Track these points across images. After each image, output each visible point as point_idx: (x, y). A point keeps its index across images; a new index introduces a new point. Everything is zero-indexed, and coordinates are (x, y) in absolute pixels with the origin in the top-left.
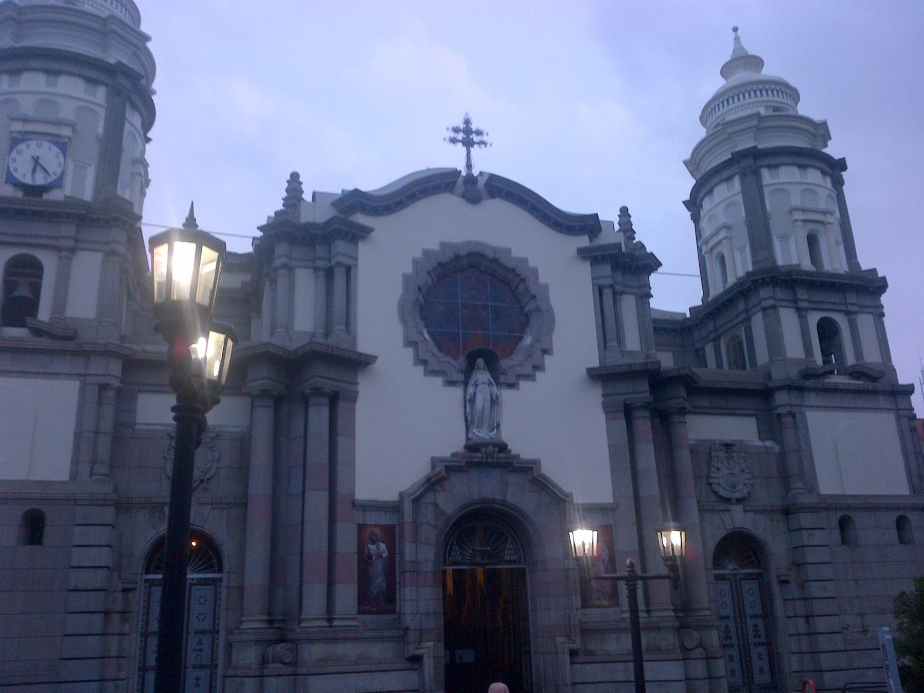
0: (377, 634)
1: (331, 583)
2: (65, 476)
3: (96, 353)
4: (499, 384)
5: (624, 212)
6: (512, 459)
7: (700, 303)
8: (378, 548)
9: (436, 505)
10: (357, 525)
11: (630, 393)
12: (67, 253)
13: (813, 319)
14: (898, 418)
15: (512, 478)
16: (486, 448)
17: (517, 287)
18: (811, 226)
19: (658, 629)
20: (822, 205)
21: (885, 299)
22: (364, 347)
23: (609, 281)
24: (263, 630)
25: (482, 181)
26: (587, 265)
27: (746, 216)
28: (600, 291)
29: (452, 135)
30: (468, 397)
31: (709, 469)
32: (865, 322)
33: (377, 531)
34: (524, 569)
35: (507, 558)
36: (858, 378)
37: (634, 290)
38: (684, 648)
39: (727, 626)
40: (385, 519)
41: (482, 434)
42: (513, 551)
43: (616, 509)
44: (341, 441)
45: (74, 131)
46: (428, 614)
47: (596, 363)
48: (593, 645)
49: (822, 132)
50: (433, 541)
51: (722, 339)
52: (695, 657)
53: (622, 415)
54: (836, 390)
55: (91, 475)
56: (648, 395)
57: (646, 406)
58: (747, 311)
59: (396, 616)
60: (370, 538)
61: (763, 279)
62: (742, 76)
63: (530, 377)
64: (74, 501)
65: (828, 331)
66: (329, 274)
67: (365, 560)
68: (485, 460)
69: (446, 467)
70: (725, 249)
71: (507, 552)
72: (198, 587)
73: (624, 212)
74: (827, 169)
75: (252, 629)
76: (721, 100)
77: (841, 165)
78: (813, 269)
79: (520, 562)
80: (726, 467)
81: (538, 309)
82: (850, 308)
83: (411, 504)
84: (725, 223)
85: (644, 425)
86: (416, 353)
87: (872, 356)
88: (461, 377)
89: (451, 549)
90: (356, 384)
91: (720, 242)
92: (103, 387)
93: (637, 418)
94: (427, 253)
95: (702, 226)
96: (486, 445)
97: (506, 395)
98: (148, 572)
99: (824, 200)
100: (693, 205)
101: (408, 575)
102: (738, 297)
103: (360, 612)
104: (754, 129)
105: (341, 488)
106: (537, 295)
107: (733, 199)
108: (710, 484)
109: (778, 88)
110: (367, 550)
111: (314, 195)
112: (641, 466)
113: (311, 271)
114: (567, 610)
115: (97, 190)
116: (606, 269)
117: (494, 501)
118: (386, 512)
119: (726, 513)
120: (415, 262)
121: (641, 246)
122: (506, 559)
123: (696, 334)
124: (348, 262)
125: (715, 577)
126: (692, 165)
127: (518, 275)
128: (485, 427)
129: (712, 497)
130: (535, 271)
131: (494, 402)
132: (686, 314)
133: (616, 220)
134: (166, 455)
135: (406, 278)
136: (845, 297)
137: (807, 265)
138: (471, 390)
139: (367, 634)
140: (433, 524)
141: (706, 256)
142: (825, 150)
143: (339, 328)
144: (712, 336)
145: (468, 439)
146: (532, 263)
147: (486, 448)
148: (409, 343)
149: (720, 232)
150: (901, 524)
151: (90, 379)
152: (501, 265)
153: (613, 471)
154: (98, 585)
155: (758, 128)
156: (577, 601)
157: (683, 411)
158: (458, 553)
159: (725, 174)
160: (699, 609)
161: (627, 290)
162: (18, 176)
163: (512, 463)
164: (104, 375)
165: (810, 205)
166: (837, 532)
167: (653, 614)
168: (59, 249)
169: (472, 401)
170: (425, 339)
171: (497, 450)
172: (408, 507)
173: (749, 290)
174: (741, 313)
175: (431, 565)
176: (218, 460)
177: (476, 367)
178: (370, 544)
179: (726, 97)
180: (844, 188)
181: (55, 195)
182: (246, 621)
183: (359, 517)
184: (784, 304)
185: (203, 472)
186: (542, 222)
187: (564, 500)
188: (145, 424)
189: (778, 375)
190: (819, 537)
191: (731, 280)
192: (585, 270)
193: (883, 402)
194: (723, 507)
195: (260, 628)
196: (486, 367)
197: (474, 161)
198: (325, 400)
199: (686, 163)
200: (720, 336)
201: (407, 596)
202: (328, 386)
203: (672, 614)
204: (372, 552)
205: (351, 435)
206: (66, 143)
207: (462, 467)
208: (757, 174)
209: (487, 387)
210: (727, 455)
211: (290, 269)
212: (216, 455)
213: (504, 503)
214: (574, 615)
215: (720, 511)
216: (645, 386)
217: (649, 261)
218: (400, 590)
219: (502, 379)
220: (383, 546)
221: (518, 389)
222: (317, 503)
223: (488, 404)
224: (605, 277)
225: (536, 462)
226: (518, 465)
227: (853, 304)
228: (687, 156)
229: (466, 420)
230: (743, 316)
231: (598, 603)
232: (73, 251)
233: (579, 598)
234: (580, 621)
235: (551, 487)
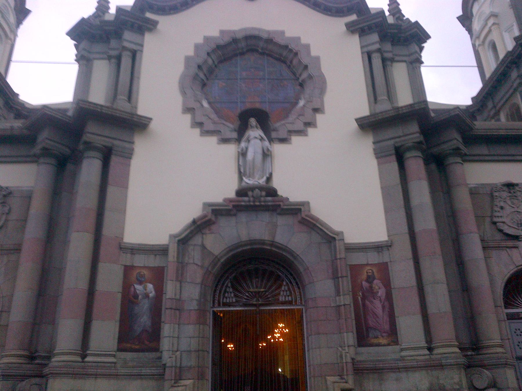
0: (135, 371)
6: (281, 201)
8: (145, 288)
9: (203, 247)
10: (123, 267)
11: (400, 137)
15: (281, 221)
16: (252, 191)
17: (291, 62)
19: (441, 367)
22: (143, 110)
26: (356, 38)
31: (492, 208)
35: (281, 299)
40: (153, 262)
42: (288, 292)
43: (390, 246)
44: (111, 191)
46: (190, 351)
47: (364, 111)
50: (199, 280)
53: (394, 158)
57: (417, 146)
60: (137, 279)
68: (252, 204)
69: (213, 211)
80: (510, 206)
81: (310, 77)
84: (492, 12)
86: (193, 118)
88: (235, 135)
89: (225, 292)
90: (133, 143)
91: (490, 31)
93: (408, 158)
94: (207, 39)
97: (278, 149)
102: (510, 68)
105: (107, 231)
106: (308, 64)
108: (495, 223)
112: (415, 202)
114: (340, 348)
117: (262, 242)
118: (156, 255)
119: (515, 250)
125: (507, 316)
127: (291, 51)
129: (498, 236)
130: (307, 47)
131: (266, 155)
135: (188, 59)
139: (123, 371)
140: (199, 264)
143: (122, 97)
146: (304, 41)
147: (252, 191)
148: (188, 110)
152: (276, 44)
156: (350, 338)
158: (232, 295)
160: (488, 347)
161: (397, 58)
167: (435, 351)
171: (264, 193)
174: (515, 80)
175: (195, 303)
176: (7, 214)
177: (249, 126)
178: (137, 284)
183: (127, 259)
186: (314, 9)
187: (334, 238)
191: (501, 56)
192: (355, 40)
194: (510, 243)
195: (15, 363)
196: (259, 126)
200: (499, 111)
202: (99, 141)
203: (457, 350)
204: (138, 292)
205: (124, 185)
207: (230, 210)
209: (258, 141)
210: (510, 194)
212: (6, 209)
213: (273, 244)
215: (507, 247)
217: (416, 29)
219: (274, 135)
220: (150, 287)
221: (290, 143)
223: (259, 157)
224: (373, 44)
225: (306, 204)
226: (285, 207)
229: (240, 172)
231: (375, 341)
234: (353, 359)
235: (319, 226)
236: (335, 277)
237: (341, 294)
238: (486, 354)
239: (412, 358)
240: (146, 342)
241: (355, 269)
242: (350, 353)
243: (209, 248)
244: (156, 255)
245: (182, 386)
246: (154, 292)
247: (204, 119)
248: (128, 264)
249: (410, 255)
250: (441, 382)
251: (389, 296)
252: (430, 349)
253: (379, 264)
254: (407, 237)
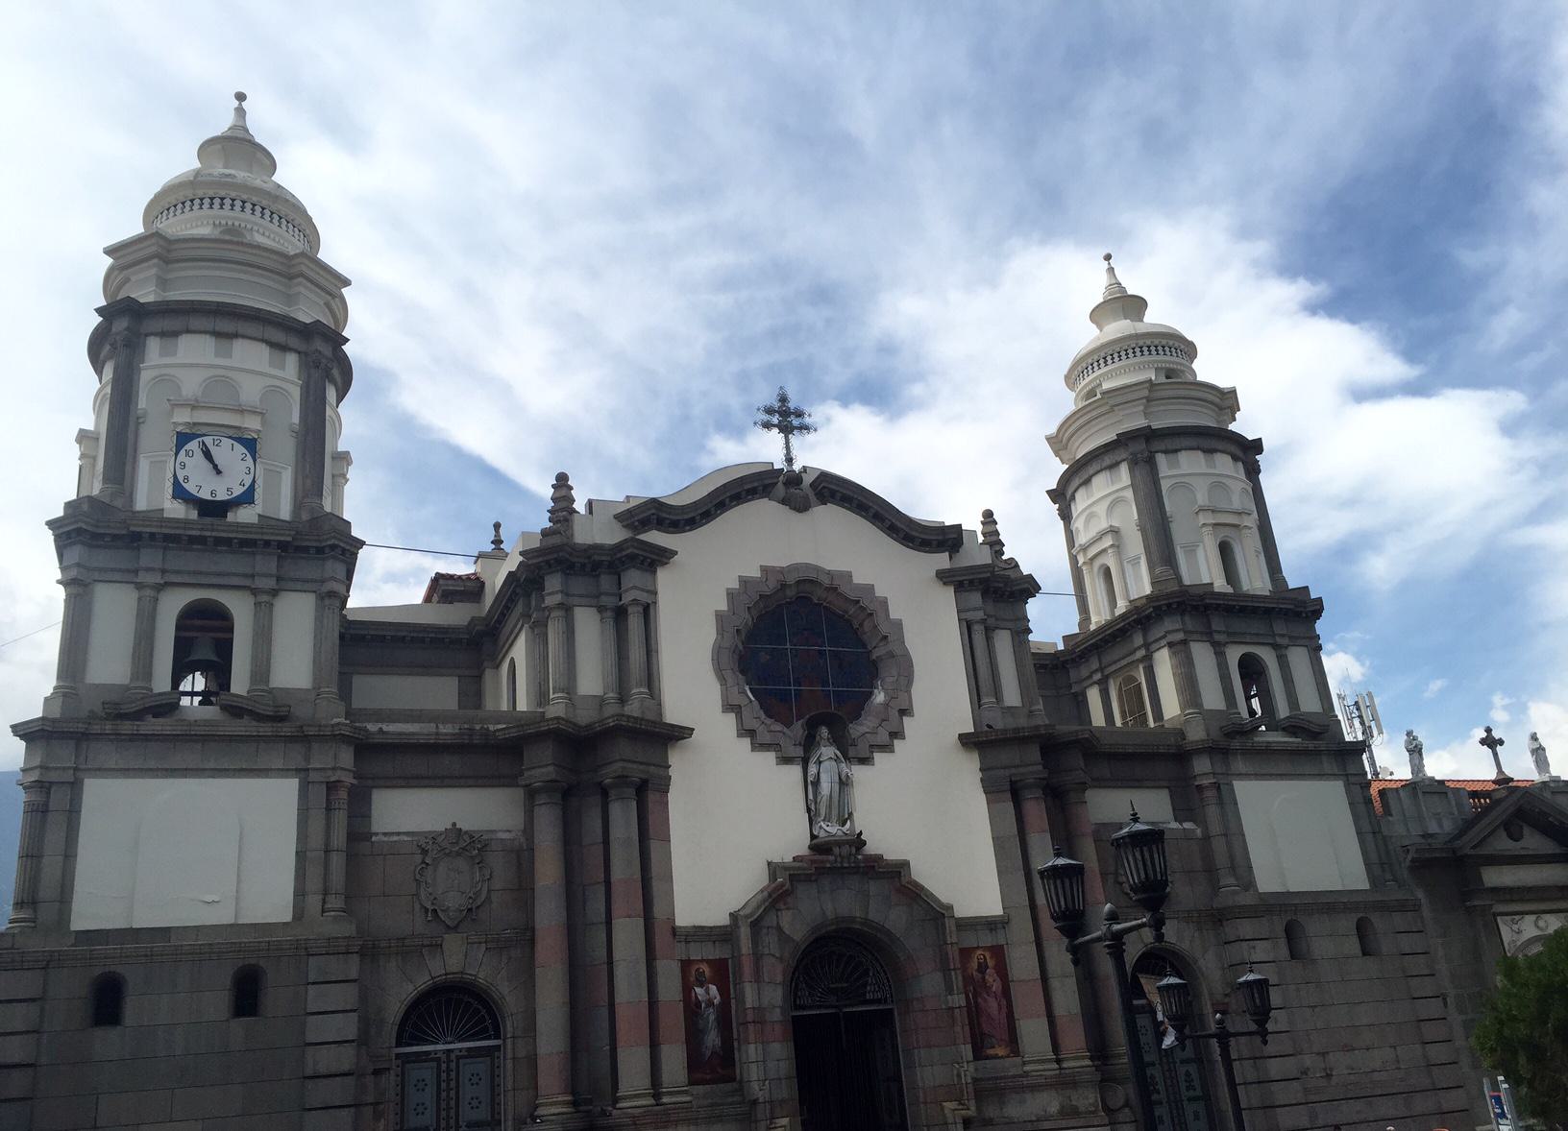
1: (654, 1045)
2: (287, 916)
3: (321, 738)
4: (847, 758)
5: (988, 517)
7: (1076, 630)
8: (707, 992)
9: (779, 929)
12: (265, 600)
13: (1234, 654)
14: (1348, 786)
15: (874, 887)
17: (861, 625)
18: (1224, 533)
20: (1236, 503)
21: (1321, 626)
22: (673, 715)
23: (980, 615)
24: (569, 1116)
25: (808, 479)
26: (949, 592)
27: (1139, 518)
28: (967, 627)
29: (766, 417)
30: (810, 779)
32: (1298, 657)
33: (705, 968)
34: (891, 1011)
36: (1294, 735)
37: (1009, 625)
38: (1109, 1111)
39: (1187, 1071)
41: (831, 829)
44: (654, 846)
45: (264, 423)
48: (991, 1112)
49: (1227, 403)
50: (779, 978)
51: (1111, 683)
52: (1121, 1120)
54: (1268, 752)
55: (323, 911)
56: (1040, 767)
58: (1147, 645)
59: (735, 1085)
61: (1169, 605)
62: (1119, 328)
63: (887, 748)
64: (303, 950)
65: (1252, 671)
66: (620, 614)
67: (692, 1009)
70: (1110, 561)
71: (868, 988)
72: (468, 1060)
73: (988, 517)
74: (1239, 453)
75: (554, 1115)
76: (1096, 358)
77: (1257, 446)
78: (1229, 590)
79: (886, 1001)
81: (891, 655)
82: (1279, 640)
83: (749, 929)
85: (1036, 811)
87: (1309, 704)
88: (799, 752)
91: (1104, 551)
92: (331, 787)
95: (1076, 525)
96: (840, 843)
97: (858, 772)
98: (399, 1044)
99: (1238, 495)
100: (1061, 496)
101: (751, 1027)
103: (692, 1083)
104: (1144, 401)
105: (658, 911)
107: (1121, 494)
109: (1171, 343)
110: (693, 995)
111: (590, 504)
113: (593, 610)
115: (298, 506)
116: (975, 598)
117: (852, 919)
118: (714, 942)
120: (731, 595)
121: (1013, 564)
122: (868, 998)
123: (1073, 674)
124: (644, 597)
126: (1058, 443)
128: (834, 818)
131: (844, 783)
132: (1056, 644)
133: (979, 528)
134: (418, 877)
135: (720, 617)
136: (1271, 626)
137: (1220, 584)
138: (812, 770)
141: (1084, 568)
142: (1232, 427)
143: (638, 691)
144: (1098, 676)
145: (813, 837)
148: (729, 707)
149: (1104, 539)
150: (1362, 929)
151: (313, 776)
153: (1001, 872)
154: (346, 1067)
155: (1149, 400)
156: (967, 1051)
157: (1083, 787)
159: (1108, 460)
162: (190, 487)
163: (874, 867)
164: (334, 769)
165: (1224, 505)
166: (1283, 942)
168: (254, 592)
169: (816, 783)
170: (751, 701)
172: (744, 932)
173: (1148, 617)
174: (1139, 648)
175: (778, 1010)
179: (1103, 354)
180: (1261, 477)
181: (245, 515)
182: (542, 1105)
183: (681, 951)
184: (1195, 637)
185: (470, 898)
187: (943, 914)
188: (385, 834)
189: (1196, 734)
190: (1261, 952)
191: (1122, 606)
193: (1328, 766)
195: (563, 1114)
197: (794, 453)
198: (631, 792)
199: (1049, 439)
201: (753, 1056)
202: (636, 773)
206: (255, 440)
207: (811, 875)
208: (1151, 462)
211: (567, 609)
214: (965, 1071)
216: (1034, 754)
217: (1026, 586)
218: (739, 1050)
219: (852, 753)
220: (713, 989)
222: (628, 936)
223: (836, 787)
226: (881, 870)
227: (1283, 636)
228: (1052, 430)
229: (809, 810)
230: (1142, 653)
231: (991, 1052)
232: (274, 593)
233: (969, 1047)
236: (945, 968)
237: (956, 992)
238: (1118, 1064)
239: (1038, 1073)
240: (720, 1070)
241: (966, 953)
242: (969, 1070)
243: (787, 932)
244: (714, 942)
245: (780, 1127)
246: (718, 997)
247: (754, 724)
248: (684, 957)
249: (1031, 936)
250: (1074, 1103)
251: (1006, 992)
252: (1058, 1061)
253: (992, 947)
254: (1028, 912)
